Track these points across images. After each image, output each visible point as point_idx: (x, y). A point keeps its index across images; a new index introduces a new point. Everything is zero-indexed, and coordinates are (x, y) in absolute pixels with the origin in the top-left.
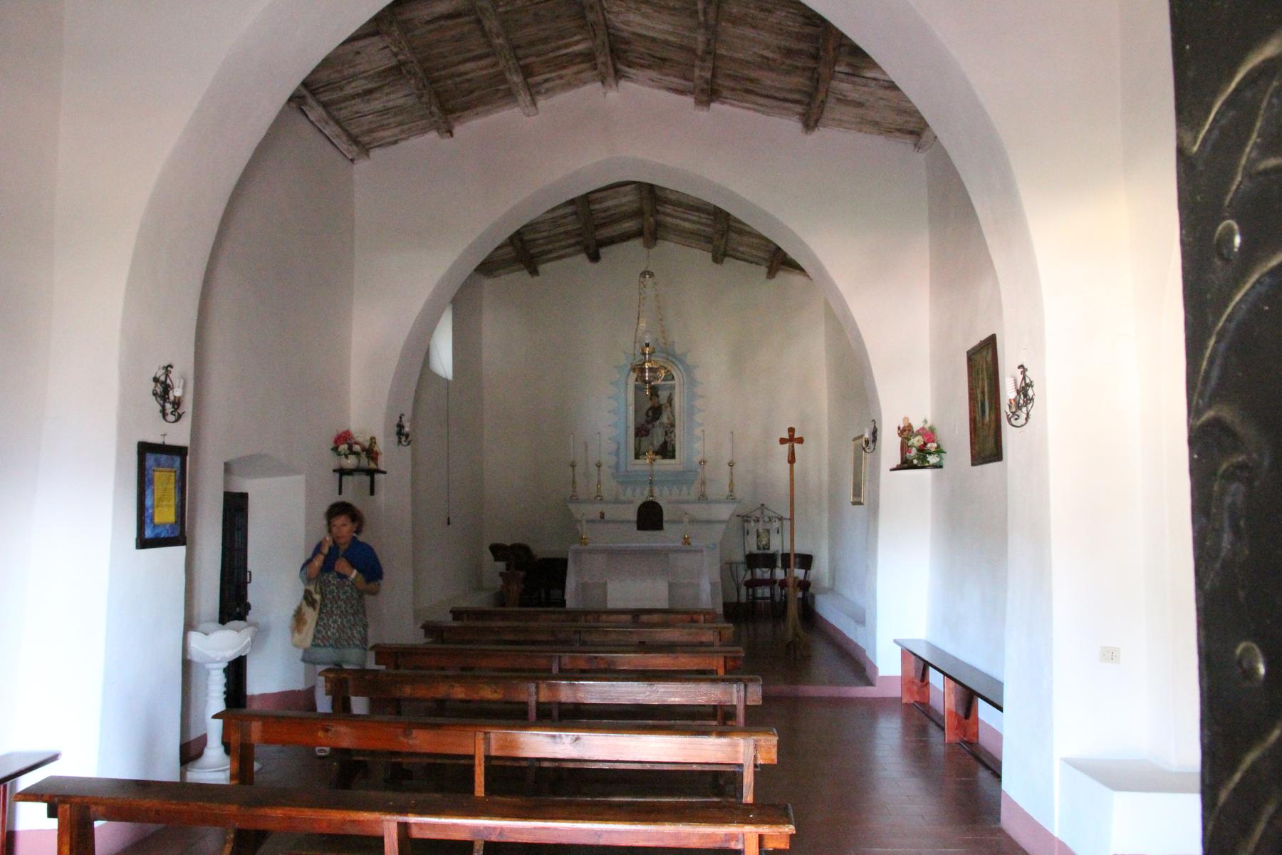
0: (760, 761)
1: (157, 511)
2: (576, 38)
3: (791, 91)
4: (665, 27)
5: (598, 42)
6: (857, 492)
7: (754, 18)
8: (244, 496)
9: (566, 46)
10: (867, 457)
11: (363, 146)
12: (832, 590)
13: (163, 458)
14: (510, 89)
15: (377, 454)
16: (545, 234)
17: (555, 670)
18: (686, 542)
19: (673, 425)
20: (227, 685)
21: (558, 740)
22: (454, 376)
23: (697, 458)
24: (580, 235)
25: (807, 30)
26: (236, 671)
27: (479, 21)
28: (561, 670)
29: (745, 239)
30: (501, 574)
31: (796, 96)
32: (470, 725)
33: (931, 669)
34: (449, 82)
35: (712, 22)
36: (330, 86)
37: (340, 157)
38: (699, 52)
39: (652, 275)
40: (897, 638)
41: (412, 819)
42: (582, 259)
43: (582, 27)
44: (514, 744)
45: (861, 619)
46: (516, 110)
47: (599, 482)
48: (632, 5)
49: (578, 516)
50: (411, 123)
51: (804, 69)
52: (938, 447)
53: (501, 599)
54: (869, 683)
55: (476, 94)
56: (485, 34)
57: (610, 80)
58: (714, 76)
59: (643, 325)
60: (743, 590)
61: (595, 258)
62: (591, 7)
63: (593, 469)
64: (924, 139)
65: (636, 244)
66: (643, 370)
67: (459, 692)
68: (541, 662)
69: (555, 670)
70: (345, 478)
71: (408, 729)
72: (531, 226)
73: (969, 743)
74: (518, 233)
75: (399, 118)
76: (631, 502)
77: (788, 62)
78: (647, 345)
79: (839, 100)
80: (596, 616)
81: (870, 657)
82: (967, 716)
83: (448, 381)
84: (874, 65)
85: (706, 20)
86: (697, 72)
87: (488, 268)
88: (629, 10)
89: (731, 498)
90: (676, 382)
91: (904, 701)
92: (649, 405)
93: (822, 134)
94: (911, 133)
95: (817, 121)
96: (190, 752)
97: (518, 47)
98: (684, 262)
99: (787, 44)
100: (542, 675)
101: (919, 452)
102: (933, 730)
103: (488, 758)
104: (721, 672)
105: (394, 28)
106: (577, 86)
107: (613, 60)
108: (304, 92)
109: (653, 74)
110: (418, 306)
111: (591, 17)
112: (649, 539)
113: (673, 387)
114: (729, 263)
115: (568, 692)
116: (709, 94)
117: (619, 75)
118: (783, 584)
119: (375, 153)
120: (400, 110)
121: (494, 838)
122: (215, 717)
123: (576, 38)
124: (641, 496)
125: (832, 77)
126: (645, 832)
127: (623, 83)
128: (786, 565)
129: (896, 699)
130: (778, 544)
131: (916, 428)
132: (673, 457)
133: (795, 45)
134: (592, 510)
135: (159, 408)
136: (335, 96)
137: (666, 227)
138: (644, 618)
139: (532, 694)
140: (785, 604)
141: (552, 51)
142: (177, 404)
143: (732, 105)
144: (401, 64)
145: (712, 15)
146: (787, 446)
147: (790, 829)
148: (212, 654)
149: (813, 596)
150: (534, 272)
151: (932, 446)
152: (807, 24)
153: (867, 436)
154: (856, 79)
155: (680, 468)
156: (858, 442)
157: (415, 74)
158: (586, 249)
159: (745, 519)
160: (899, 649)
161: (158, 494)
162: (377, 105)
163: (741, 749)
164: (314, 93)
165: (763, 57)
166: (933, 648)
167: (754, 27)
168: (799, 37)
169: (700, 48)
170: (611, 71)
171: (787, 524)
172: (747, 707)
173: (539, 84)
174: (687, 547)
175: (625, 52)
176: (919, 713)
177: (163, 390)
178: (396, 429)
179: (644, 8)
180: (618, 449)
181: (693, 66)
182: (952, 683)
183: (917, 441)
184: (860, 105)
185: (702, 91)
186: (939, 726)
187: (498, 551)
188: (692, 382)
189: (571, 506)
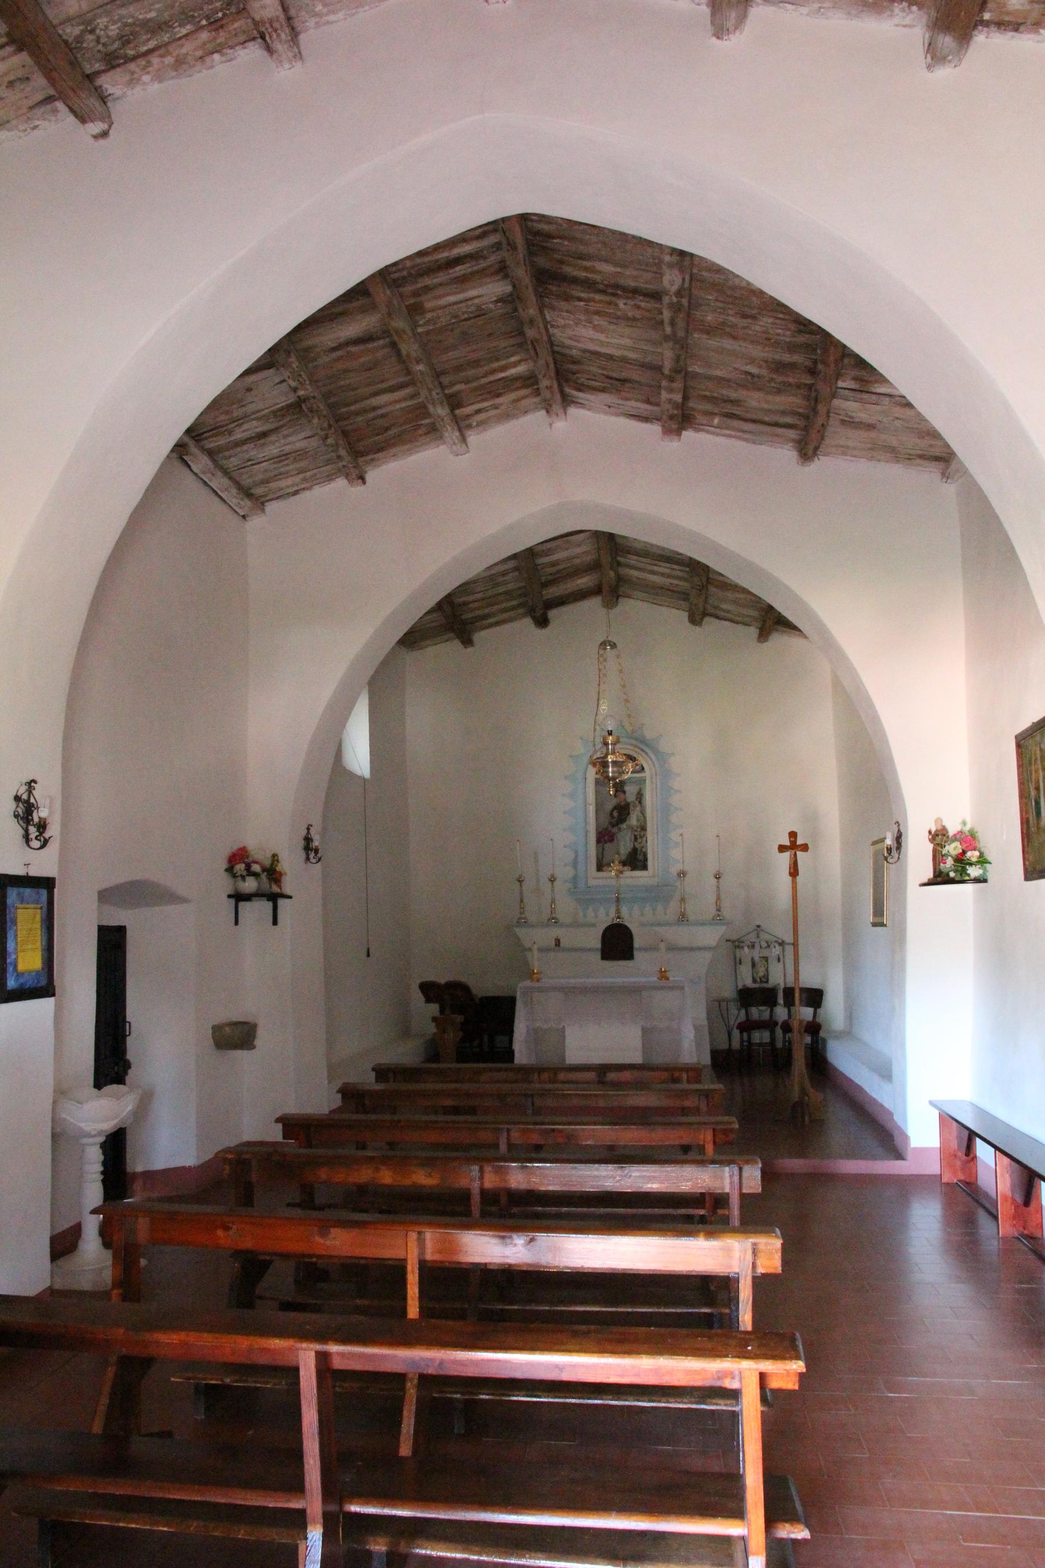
0: (760, 1270)
1: (21, 955)
2: (513, 359)
3: (783, 413)
4: (627, 342)
5: (541, 362)
6: (878, 910)
7: (734, 326)
8: (121, 930)
9: (504, 369)
10: (890, 871)
11: (257, 499)
12: (848, 1034)
13: (28, 891)
14: (433, 424)
15: (281, 874)
16: (479, 596)
17: (503, 1148)
18: (663, 975)
19: (643, 828)
20: (104, 1164)
21: (508, 1241)
23: (674, 870)
24: (525, 595)
25: (801, 339)
26: (115, 1145)
27: (394, 345)
28: (510, 1146)
29: (729, 595)
30: (434, 1019)
31: (788, 420)
32: (401, 1223)
33: (978, 1140)
34: (360, 419)
35: (681, 334)
36: (216, 430)
37: (230, 515)
38: (666, 372)
39: (614, 646)
40: (934, 1098)
41: (334, 1348)
42: (527, 622)
43: (520, 345)
44: (453, 1247)
45: (886, 1072)
46: (443, 447)
47: (553, 901)
48: (583, 317)
49: (527, 945)
50: (312, 470)
52: (981, 855)
53: (433, 1052)
54: (899, 1156)
57: (557, 408)
58: (686, 398)
59: (604, 707)
60: (736, 1033)
61: (542, 622)
62: (531, 321)
63: (546, 886)
64: (953, 466)
66: (604, 764)
67: (387, 1177)
68: (485, 1136)
69: (503, 1148)
70: (241, 904)
71: (324, 1228)
72: (465, 588)
73: (1031, 1238)
74: (449, 596)
75: (303, 464)
76: (594, 925)
77: (781, 379)
78: (610, 733)
79: (843, 422)
80: (554, 1071)
81: (899, 1122)
82: (1027, 1202)
83: (364, 779)
84: (883, 380)
85: (674, 333)
86: (664, 395)
87: (413, 639)
89: (718, 919)
90: (647, 774)
91: (945, 1180)
92: (614, 802)
93: (823, 465)
94: (937, 459)
95: (816, 449)
96: (63, 1245)
98: (653, 624)
99: (777, 357)
100: (487, 1154)
101: (956, 864)
102: (983, 1218)
103: (423, 1264)
104: (710, 1148)
105: (293, 359)
107: (560, 386)
108: (187, 439)
110: (327, 691)
111: (530, 333)
112: (617, 973)
113: (643, 781)
114: (711, 625)
115: (519, 1177)
116: (681, 421)
117: (567, 401)
118: (787, 1028)
119: (270, 507)
120: (300, 454)
121: (431, 1371)
122: (94, 1212)
124: (605, 917)
125: (834, 396)
126: (619, 1366)
127: (572, 411)
128: (789, 1002)
129: (935, 1176)
130: (778, 977)
131: (951, 832)
132: (645, 867)
133: (787, 358)
134: (543, 936)
135: (21, 832)
136: (222, 441)
138: (612, 1076)
139: (476, 1178)
140: (788, 1051)
141: (485, 376)
142: (42, 826)
143: (708, 432)
144: (299, 403)
145: (681, 323)
146: (787, 855)
147: (798, 1366)
148: (88, 1127)
149: (824, 1041)
150: (467, 642)
151: (972, 855)
152: (800, 331)
153: (889, 842)
154: (865, 396)
155: (655, 881)
156: (879, 846)
158: (531, 612)
159: (737, 944)
160: (937, 1112)
161: (21, 934)
162: (273, 449)
163: (737, 1254)
166: (981, 1113)
167: (735, 338)
168: (792, 348)
169: (668, 366)
170: (558, 397)
171: (789, 950)
172: (743, 1197)
173: (468, 416)
174: (663, 983)
175: (578, 372)
176: (965, 1199)
177: (26, 811)
178: (302, 843)
179: (597, 320)
180: (576, 857)
182: (1006, 1160)
183: (953, 849)
184: (871, 427)
185: (671, 417)
186: (990, 1213)
187: (429, 990)
188: (666, 774)
189: (521, 932)
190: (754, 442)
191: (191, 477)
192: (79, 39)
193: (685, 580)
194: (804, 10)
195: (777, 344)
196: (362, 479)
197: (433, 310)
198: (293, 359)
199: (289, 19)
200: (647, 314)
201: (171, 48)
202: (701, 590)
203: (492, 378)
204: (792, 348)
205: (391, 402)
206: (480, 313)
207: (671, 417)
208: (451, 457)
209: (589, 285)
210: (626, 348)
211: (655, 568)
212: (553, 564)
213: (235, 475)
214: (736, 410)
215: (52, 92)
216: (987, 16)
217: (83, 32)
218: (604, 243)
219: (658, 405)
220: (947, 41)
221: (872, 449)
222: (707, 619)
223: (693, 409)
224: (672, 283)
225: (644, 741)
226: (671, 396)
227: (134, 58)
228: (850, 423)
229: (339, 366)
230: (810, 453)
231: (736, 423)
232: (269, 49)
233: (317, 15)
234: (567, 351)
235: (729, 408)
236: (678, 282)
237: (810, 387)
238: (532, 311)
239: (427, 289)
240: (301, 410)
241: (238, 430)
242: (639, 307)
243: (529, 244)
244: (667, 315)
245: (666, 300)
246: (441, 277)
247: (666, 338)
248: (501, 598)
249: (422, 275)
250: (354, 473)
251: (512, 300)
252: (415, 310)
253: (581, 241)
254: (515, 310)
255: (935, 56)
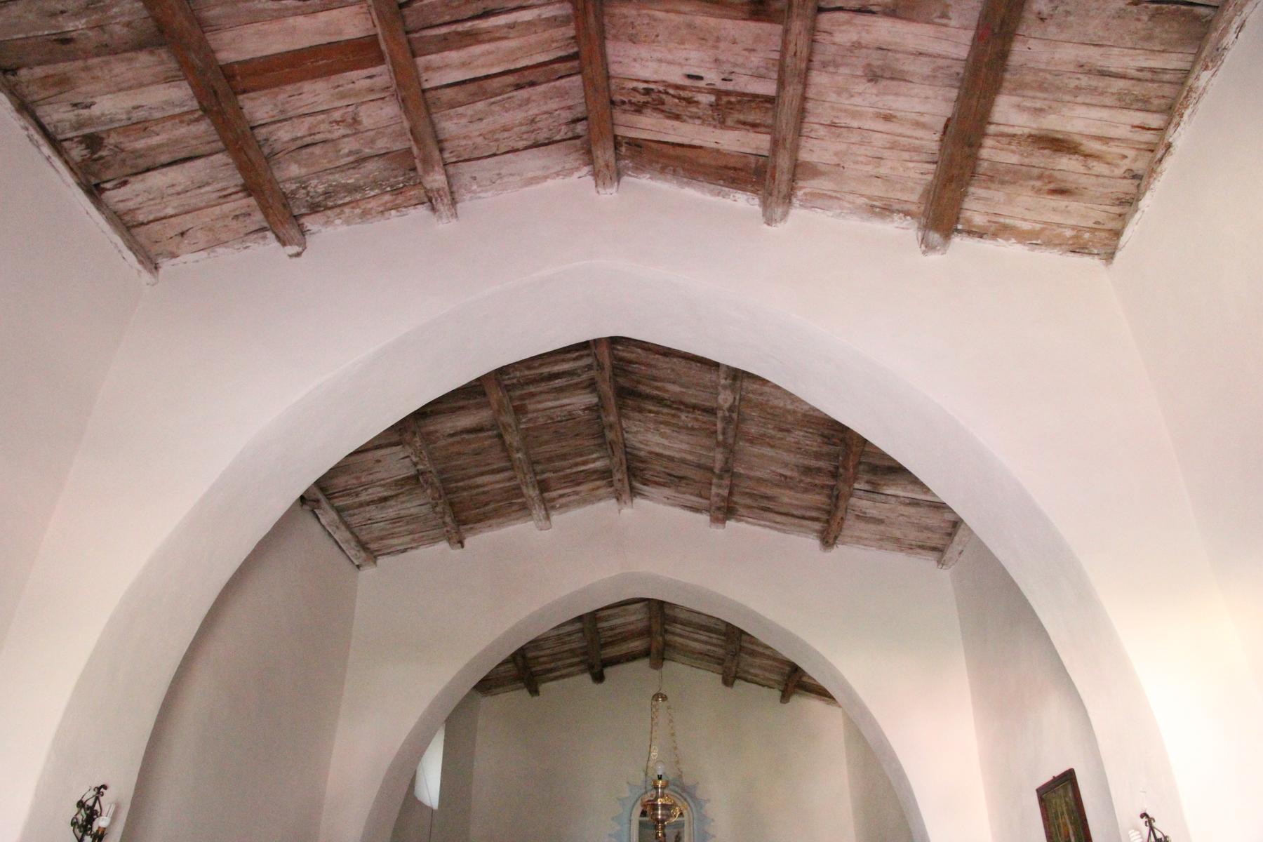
2: (595, 456)
4: (685, 446)
5: (616, 459)
7: (772, 437)
9: (585, 463)
11: (372, 552)
16: (548, 652)
22: (440, 806)
25: (825, 449)
27: (500, 436)
29: (758, 661)
31: (814, 514)
34: (465, 494)
36: (346, 492)
38: (717, 471)
39: (665, 698)
42: (587, 678)
43: (600, 445)
48: (652, 426)
50: (422, 532)
51: (822, 487)
55: (491, 506)
56: (505, 447)
58: (731, 493)
59: (654, 754)
61: (599, 678)
62: (611, 427)
64: (948, 555)
65: (642, 665)
72: (535, 644)
75: (411, 527)
77: (809, 480)
78: (660, 777)
85: (725, 439)
86: (714, 490)
87: (487, 685)
88: (647, 430)
90: (686, 818)
94: (934, 549)
95: (836, 538)
97: (537, 462)
98: (693, 683)
99: (806, 462)
105: (417, 439)
106: (592, 502)
109: (667, 492)
110: (410, 721)
111: (610, 435)
116: (725, 511)
117: (634, 493)
119: (381, 560)
120: (413, 519)
123: (595, 456)
125: (851, 495)
127: (638, 501)
133: (813, 463)
137: (675, 647)
143: (747, 522)
145: (731, 433)
150: (534, 691)
154: (875, 496)
157: (432, 484)
162: (391, 512)
164: (329, 497)
165: (781, 475)
167: (772, 447)
168: (818, 456)
169: (718, 467)
170: (627, 488)
173: (553, 500)
175: (644, 469)
179: (663, 429)
181: (711, 484)
184: (881, 522)
185: (719, 509)
190: (784, 532)
191: (319, 526)
192: (294, 192)
193: (721, 646)
194: (830, 214)
195: (806, 453)
196: (461, 543)
197: (534, 412)
198: (417, 439)
199: (452, 193)
200: (704, 426)
201: (361, 203)
202: (735, 653)
203: (575, 470)
204: (818, 456)
205: (492, 482)
206: (571, 416)
207: (719, 509)
208: (538, 532)
209: (659, 401)
210: (685, 451)
211: (696, 636)
212: (612, 629)
213: (356, 530)
214: (771, 505)
215: (265, 224)
216: (960, 227)
217: (298, 188)
218: (673, 370)
219: (708, 499)
220: (935, 237)
221: (881, 540)
222: (737, 682)
223: (736, 503)
224: (725, 400)
225: (684, 789)
226: (720, 491)
227: (331, 208)
228: (862, 517)
229: (455, 449)
230: (831, 541)
231: (771, 515)
232: (433, 209)
233: (471, 192)
234: (635, 452)
235: (765, 503)
236: (730, 400)
237: (832, 488)
238: (612, 419)
239: (533, 395)
240: (418, 480)
241: (364, 493)
242: (697, 420)
243: (614, 367)
244: (720, 426)
245: (720, 414)
246: (543, 386)
247: (718, 444)
248: (565, 655)
249: (527, 384)
250: (456, 538)
251: (596, 410)
252: (519, 410)
253: (655, 367)
254: (599, 417)
255: (928, 247)
